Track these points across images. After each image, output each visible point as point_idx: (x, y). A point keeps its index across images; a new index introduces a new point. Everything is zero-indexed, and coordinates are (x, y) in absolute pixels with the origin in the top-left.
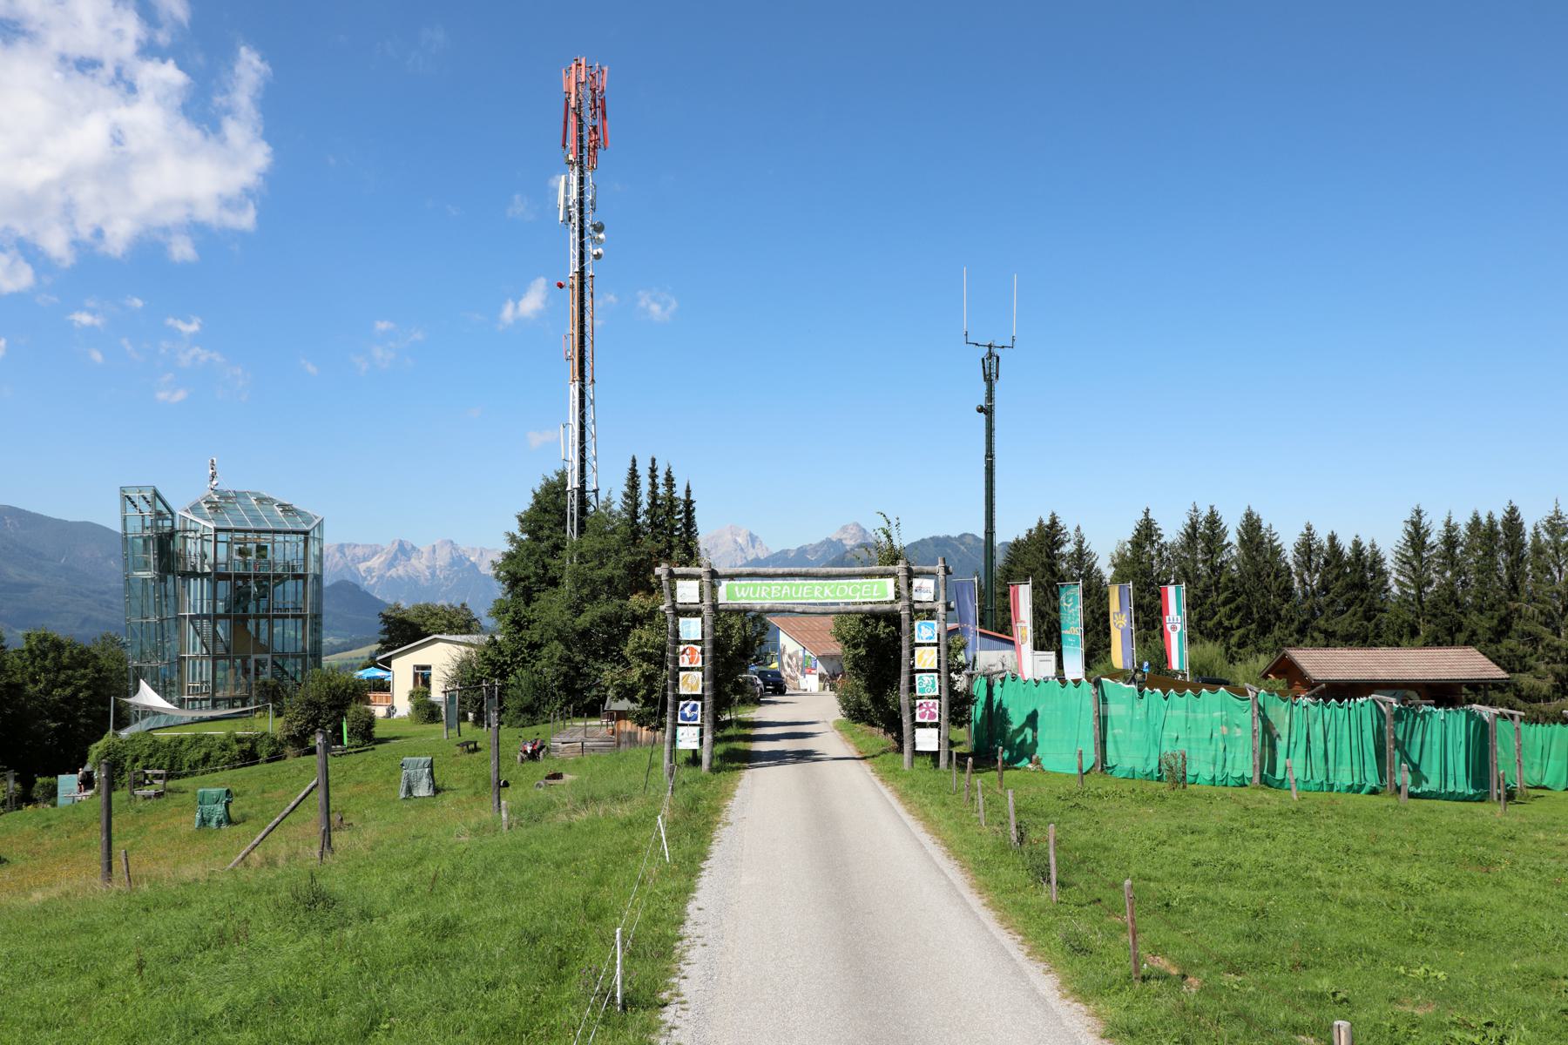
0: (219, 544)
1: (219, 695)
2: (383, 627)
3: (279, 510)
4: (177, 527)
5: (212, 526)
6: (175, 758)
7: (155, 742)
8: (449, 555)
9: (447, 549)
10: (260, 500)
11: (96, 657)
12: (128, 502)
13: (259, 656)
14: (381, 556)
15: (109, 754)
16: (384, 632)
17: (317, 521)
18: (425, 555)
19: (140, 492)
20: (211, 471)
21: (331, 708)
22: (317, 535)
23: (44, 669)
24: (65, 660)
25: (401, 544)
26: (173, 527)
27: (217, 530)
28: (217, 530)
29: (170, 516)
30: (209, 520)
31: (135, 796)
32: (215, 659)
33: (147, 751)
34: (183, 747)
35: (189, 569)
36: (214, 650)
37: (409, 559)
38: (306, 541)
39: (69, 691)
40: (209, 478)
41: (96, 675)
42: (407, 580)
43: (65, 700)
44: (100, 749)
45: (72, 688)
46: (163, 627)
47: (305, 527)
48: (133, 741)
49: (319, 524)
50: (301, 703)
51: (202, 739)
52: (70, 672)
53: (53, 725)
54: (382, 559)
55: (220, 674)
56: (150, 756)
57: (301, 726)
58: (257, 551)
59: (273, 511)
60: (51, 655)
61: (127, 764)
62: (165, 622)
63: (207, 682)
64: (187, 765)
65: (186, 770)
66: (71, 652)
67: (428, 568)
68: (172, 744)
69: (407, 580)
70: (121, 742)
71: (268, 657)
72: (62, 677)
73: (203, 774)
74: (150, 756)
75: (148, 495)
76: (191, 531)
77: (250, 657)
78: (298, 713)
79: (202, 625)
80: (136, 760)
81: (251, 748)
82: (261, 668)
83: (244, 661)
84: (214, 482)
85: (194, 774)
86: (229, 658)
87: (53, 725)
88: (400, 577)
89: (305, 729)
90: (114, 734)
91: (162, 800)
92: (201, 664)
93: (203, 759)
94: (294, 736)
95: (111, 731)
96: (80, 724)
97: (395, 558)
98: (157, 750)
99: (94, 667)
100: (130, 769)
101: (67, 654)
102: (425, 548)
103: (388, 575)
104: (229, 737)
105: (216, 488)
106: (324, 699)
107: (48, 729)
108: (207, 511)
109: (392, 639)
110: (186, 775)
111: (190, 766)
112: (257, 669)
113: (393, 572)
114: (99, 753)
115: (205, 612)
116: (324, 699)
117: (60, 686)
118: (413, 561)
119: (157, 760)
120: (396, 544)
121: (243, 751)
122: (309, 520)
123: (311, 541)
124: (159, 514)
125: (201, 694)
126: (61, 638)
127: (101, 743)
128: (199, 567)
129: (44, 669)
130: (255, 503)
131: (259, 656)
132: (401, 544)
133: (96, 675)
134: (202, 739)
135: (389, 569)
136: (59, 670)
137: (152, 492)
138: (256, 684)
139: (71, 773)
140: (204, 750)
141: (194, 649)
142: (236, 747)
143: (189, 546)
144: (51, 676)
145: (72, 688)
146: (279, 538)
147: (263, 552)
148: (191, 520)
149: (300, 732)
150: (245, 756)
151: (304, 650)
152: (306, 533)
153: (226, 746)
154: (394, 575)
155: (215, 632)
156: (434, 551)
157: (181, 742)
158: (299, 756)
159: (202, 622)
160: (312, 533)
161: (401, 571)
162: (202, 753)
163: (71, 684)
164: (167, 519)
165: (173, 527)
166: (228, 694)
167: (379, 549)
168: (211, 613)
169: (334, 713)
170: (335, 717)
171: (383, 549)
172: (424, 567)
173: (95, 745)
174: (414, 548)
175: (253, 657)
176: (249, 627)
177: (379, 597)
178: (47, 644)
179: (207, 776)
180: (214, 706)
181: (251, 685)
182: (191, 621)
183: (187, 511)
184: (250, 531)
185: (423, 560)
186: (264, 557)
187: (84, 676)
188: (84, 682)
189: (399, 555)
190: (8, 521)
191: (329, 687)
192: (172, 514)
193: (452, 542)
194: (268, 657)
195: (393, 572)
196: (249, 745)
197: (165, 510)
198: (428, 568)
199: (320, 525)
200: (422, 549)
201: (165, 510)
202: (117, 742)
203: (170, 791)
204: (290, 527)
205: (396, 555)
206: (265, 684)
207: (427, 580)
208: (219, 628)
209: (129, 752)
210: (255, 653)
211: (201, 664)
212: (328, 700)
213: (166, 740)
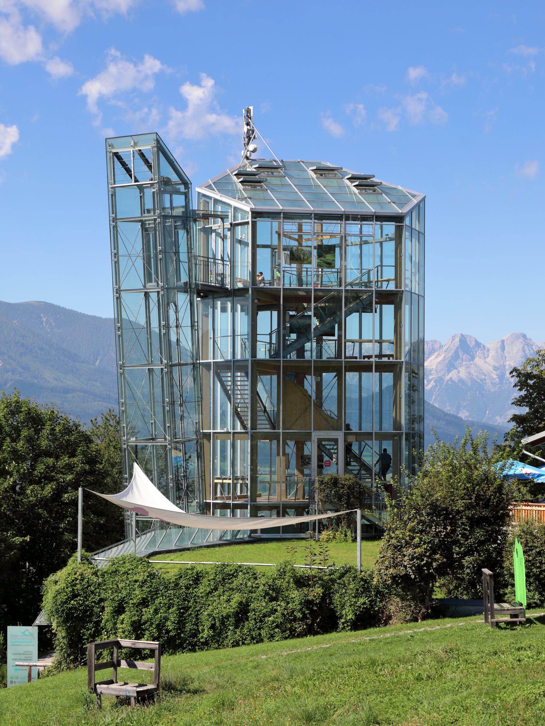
0: (259, 250)
1: (262, 500)
2: (518, 394)
3: (351, 185)
4: (194, 206)
5: (247, 207)
6: (187, 609)
7: (152, 576)
8: (521, 354)
9: (518, 345)
10: (321, 171)
11: (88, 440)
12: (118, 164)
13: (324, 434)
14: (439, 355)
15: (75, 596)
16: (519, 402)
17: (415, 201)
18: (492, 353)
19: (136, 144)
20: (246, 128)
21: (475, 522)
22: (416, 225)
23: (16, 456)
24: (44, 443)
25: (463, 340)
26: (187, 206)
27: (256, 214)
28: (256, 214)
29: (182, 188)
30: (241, 199)
31: (99, 695)
32: (254, 438)
33: (138, 594)
34: (202, 589)
35: (213, 281)
36: (254, 427)
37: (473, 358)
38: (398, 238)
39: (48, 490)
40: (243, 141)
41: (87, 467)
42: (469, 384)
43: (44, 503)
44: (62, 585)
45: (53, 485)
46: (171, 379)
47: (396, 210)
48: (116, 572)
49: (418, 205)
50: (418, 511)
51: (233, 576)
52: (50, 461)
53: (18, 540)
54: (440, 358)
55: (263, 470)
56: (144, 603)
57: (420, 557)
58: (319, 256)
59: (342, 187)
60: (25, 433)
61: (106, 616)
62: (176, 369)
63: (243, 479)
64: (208, 624)
65: (206, 633)
66: (53, 430)
67: (496, 368)
68: (183, 582)
69: (469, 384)
70: (95, 574)
71: (339, 435)
72: (40, 468)
73: (236, 644)
74: (144, 603)
75: (148, 147)
76: (215, 216)
77: (308, 436)
78: (412, 530)
79: (234, 382)
80: (119, 610)
81: (323, 598)
82: (326, 458)
83: (300, 446)
84: (251, 147)
85: (220, 645)
86: (276, 437)
87: (18, 540)
88: (461, 380)
89: (429, 565)
90: (84, 558)
91: (151, 710)
92: (233, 446)
93: (236, 614)
94: (407, 576)
95: (79, 552)
96: (433, 599)
97: (456, 356)
98: (154, 594)
99: (84, 453)
100: (109, 626)
101: (46, 432)
102: (491, 344)
103: (448, 377)
104: (282, 573)
105: (254, 156)
106: (460, 504)
107: (10, 547)
108: (240, 186)
109: (535, 414)
110: (206, 645)
111: (213, 627)
112: (320, 459)
113: (453, 375)
114: (58, 593)
115: (239, 357)
116: (460, 504)
117: (38, 483)
118: (477, 360)
119: (156, 611)
120: (457, 339)
121: (308, 603)
122: (402, 199)
123: (406, 234)
124: (166, 182)
125: (235, 498)
126: (43, 410)
127: (61, 575)
128: (228, 280)
129: (16, 456)
130: (314, 176)
131: (324, 434)
132: (463, 340)
133: (87, 467)
134: (233, 576)
135: (449, 371)
136: (35, 459)
137: (154, 144)
138: (321, 483)
139: (25, 624)
140: (237, 598)
141: (223, 423)
142: (296, 595)
143: (213, 245)
144: (25, 466)
145: (53, 485)
146: (353, 228)
147: (329, 257)
148: (216, 201)
149: (419, 569)
150: (312, 611)
151: (397, 425)
152: (398, 219)
153: (278, 590)
154: (455, 378)
155: (255, 394)
156: (503, 348)
157: (197, 579)
158: (415, 620)
159: (234, 377)
160: (407, 221)
161: (463, 373)
162: (234, 603)
163: (51, 479)
164: (178, 192)
165: (187, 206)
166: (275, 499)
167: (437, 346)
168: (248, 356)
169: (479, 533)
170: (482, 543)
171: (441, 346)
172: (491, 369)
173: (52, 578)
174: (478, 344)
175: (316, 435)
176: (307, 386)
177: (436, 405)
178: (21, 417)
179: (243, 649)
180: (254, 514)
181: (312, 483)
182: (217, 375)
183: (209, 187)
184: (307, 216)
185: (489, 360)
186: (330, 265)
187: (70, 468)
188: (69, 477)
189: (461, 353)
190: (44, 320)
191: (469, 479)
192: (186, 183)
193: (524, 336)
194: (339, 435)
195: (453, 375)
196: (319, 590)
197: (174, 178)
198: (496, 368)
199: (420, 207)
200: (488, 346)
201: (174, 178)
202: (88, 573)
203: (170, 687)
204: (372, 209)
205: (456, 352)
206: (335, 482)
207: (494, 384)
208: (260, 388)
209: (108, 595)
210: (317, 428)
211: (233, 446)
212: (468, 507)
213: (171, 575)
